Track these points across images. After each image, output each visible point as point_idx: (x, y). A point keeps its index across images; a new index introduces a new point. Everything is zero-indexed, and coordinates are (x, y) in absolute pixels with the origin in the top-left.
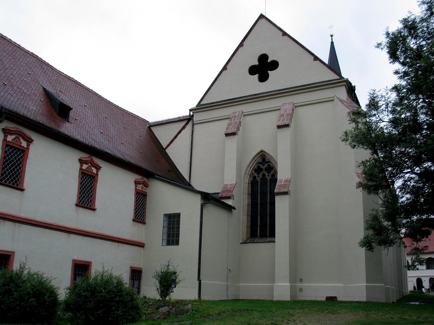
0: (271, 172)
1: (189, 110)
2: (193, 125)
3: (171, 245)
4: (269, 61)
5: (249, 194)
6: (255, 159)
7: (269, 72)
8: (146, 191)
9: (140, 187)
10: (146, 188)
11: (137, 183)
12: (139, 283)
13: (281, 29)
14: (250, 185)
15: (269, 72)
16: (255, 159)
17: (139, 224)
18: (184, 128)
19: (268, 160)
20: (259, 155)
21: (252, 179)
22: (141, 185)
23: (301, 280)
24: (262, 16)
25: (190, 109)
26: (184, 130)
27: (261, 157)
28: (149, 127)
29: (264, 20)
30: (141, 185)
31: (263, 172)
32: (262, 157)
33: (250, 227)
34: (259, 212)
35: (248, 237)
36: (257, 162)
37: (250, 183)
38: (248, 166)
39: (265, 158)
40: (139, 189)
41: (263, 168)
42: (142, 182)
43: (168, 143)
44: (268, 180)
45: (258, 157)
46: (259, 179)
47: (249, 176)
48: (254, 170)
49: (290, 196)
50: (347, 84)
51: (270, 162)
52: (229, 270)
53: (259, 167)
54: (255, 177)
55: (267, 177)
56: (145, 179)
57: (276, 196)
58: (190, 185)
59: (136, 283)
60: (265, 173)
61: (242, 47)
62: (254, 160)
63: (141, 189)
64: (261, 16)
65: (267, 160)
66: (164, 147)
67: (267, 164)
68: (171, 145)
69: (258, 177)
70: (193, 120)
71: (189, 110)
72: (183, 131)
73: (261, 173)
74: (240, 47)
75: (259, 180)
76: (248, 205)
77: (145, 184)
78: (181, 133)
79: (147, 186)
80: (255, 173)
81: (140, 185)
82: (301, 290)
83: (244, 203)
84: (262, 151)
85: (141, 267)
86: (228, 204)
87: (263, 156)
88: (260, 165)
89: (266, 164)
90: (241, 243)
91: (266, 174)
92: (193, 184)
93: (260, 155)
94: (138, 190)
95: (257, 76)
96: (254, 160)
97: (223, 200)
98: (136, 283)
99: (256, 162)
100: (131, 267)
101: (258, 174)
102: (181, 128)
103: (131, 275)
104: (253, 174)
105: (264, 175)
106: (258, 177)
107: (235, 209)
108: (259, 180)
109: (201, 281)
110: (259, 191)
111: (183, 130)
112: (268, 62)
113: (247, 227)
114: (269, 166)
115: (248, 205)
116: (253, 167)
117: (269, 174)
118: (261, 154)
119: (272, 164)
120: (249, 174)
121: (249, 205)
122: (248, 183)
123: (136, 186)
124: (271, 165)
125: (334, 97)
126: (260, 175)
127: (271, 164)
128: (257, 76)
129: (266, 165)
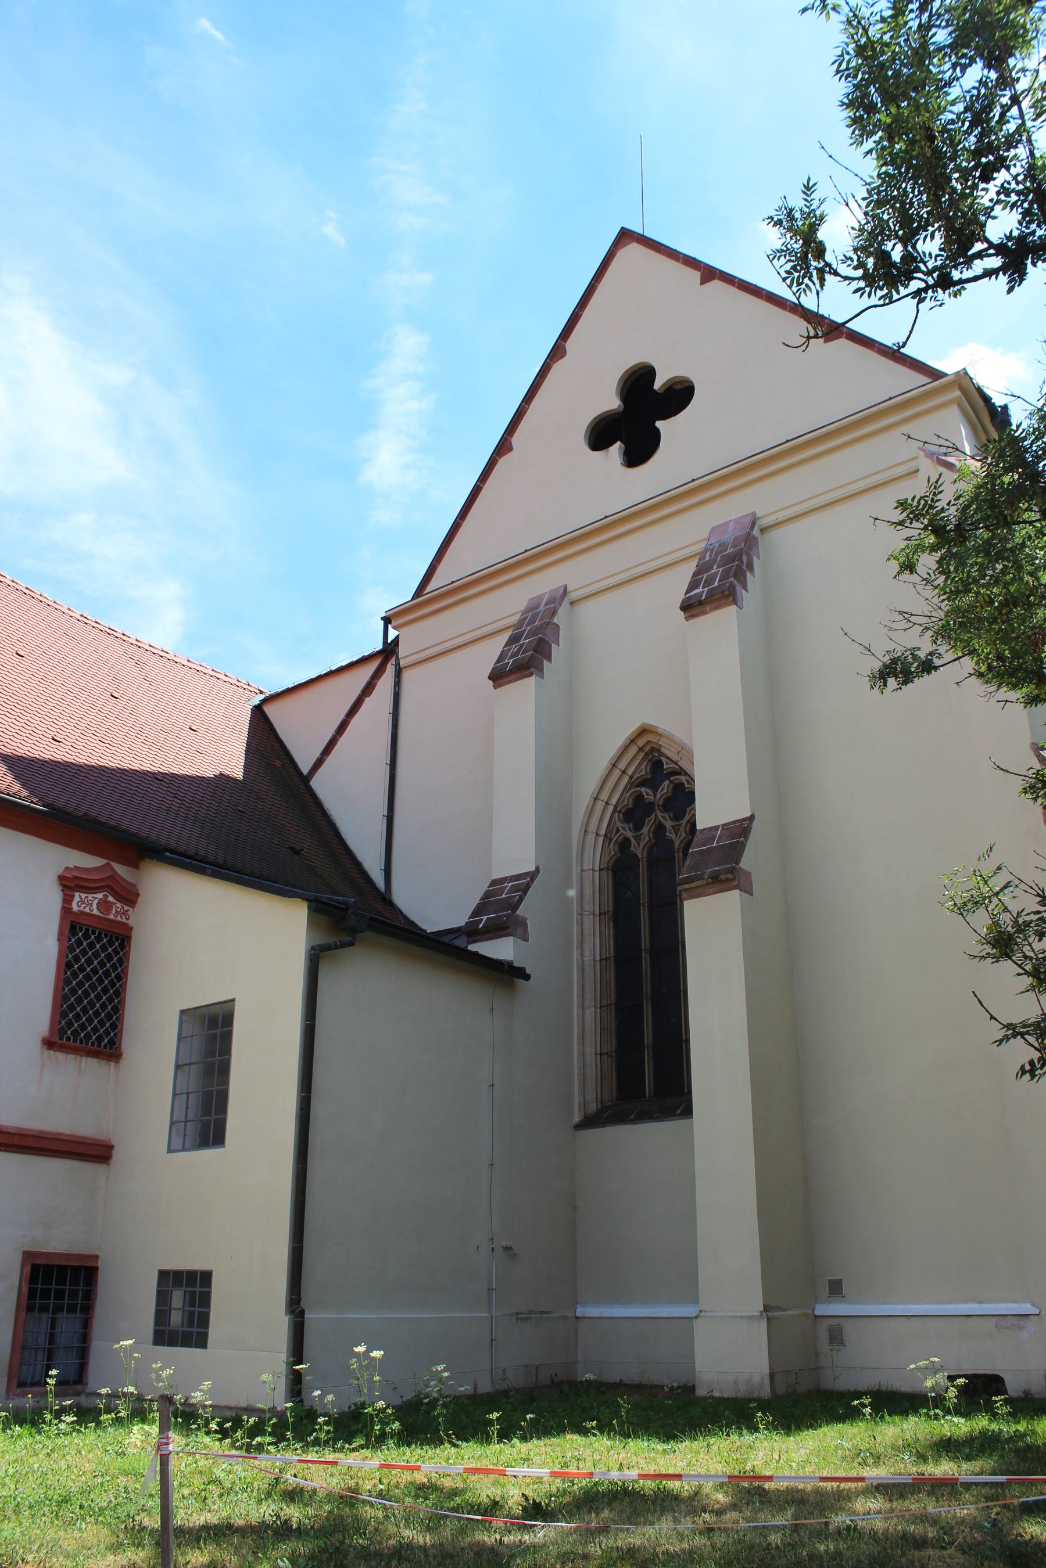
0: (688, 809)
1: (382, 619)
2: (398, 673)
3: (212, 1145)
4: (657, 385)
5: (604, 913)
6: (622, 765)
7: (659, 424)
8: (126, 921)
9: (87, 903)
10: (126, 908)
11: (73, 885)
12: (87, 1324)
13: (695, 259)
14: (608, 876)
15: (659, 424)
16: (622, 765)
17: (84, 1059)
18: (368, 689)
19: (673, 765)
20: (634, 750)
21: (613, 848)
22: (100, 896)
23: (836, 1289)
24: (625, 236)
25: (384, 615)
26: (370, 697)
27: (642, 755)
28: (258, 712)
29: (633, 249)
30: (96, 896)
31: (653, 815)
32: (647, 754)
33: (614, 1054)
34: (647, 988)
35: (606, 1097)
36: (631, 777)
37: (608, 868)
38: (595, 799)
39: (662, 758)
40: (87, 910)
41: (653, 798)
42: (107, 883)
43: (317, 755)
44: (676, 847)
45: (634, 758)
46: (642, 845)
47: (601, 839)
48: (620, 812)
49: (752, 896)
50: (964, 396)
51: (681, 772)
52: (507, 1249)
53: (639, 798)
54: (625, 844)
55: (670, 835)
56: (120, 869)
57: (686, 903)
58: (386, 899)
59: (68, 1325)
60: (662, 820)
61: (560, 359)
62: (617, 773)
63: (95, 912)
64: (621, 238)
65: (667, 764)
66: (305, 769)
67: (671, 782)
68: (329, 760)
69: (638, 838)
70: (398, 659)
71: (382, 619)
72: (368, 701)
73: (646, 822)
74: (554, 363)
75: (639, 849)
76: (601, 960)
77: (118, 890)
78: (358, 710)
79: (129, 897)
80: (626, 826)
81: (90, 896)
82: (836, 1336)
83: (582, 955)
84: (644, 731)
85: (90, 1253)
86: (480, 952)
87: (653, 750)
88: (643, 789)
89: (667, 782)
90: (578, 1127)
91: (668, 824)
92: (405, 898)
93: (641, 749)
94: (75, 914)
95: (616, 449)
96: (617, 773)
97: (472, 947)
98: (68, 1325)
99: (626, 779)
100: (27, 1255)
101: (638, 827)
102: (358, 692)
103: (25, 1289)
104: (618, 830)
105: (660, 828)
106: (638, 838)
107: (527, 977)
108: (639, 849)
109: (302, 1312)
110: (644, 898)
111: (367, 699)
112: (654, 390)
113: (601, 1054)
114: (679, 788)
115: (604, 961)
116: (614, 801)
117: (680, 820)
118: (641, 742)
119: (689, 779)
120: (603, 832)
121: (607, 959)
122: (600, 870)
123: (67, 900)
124: (685, 783)
125: (916, 458)
126: (645, 830)
127: (683, 778)
128: (616, 449)
129: (665, 787)
